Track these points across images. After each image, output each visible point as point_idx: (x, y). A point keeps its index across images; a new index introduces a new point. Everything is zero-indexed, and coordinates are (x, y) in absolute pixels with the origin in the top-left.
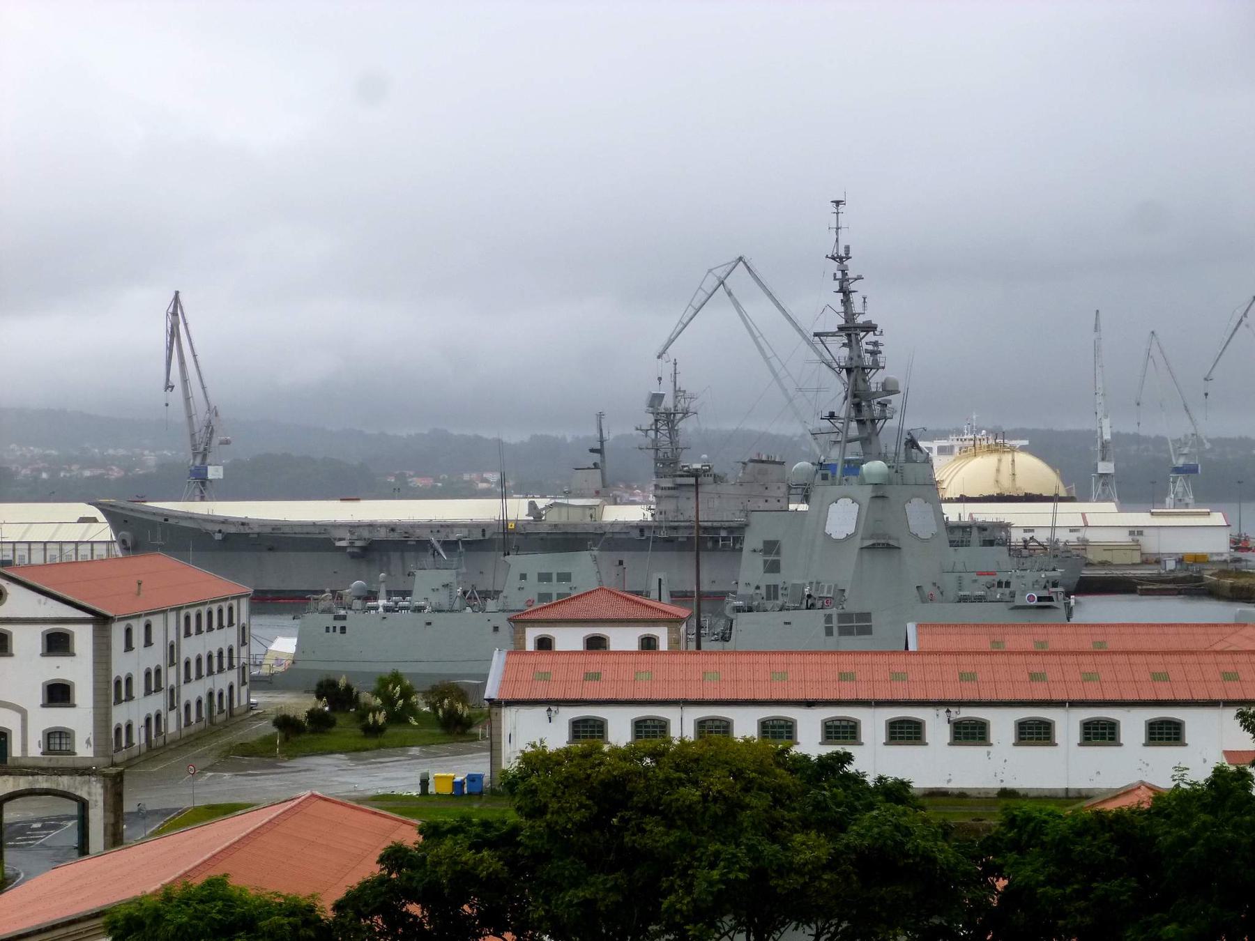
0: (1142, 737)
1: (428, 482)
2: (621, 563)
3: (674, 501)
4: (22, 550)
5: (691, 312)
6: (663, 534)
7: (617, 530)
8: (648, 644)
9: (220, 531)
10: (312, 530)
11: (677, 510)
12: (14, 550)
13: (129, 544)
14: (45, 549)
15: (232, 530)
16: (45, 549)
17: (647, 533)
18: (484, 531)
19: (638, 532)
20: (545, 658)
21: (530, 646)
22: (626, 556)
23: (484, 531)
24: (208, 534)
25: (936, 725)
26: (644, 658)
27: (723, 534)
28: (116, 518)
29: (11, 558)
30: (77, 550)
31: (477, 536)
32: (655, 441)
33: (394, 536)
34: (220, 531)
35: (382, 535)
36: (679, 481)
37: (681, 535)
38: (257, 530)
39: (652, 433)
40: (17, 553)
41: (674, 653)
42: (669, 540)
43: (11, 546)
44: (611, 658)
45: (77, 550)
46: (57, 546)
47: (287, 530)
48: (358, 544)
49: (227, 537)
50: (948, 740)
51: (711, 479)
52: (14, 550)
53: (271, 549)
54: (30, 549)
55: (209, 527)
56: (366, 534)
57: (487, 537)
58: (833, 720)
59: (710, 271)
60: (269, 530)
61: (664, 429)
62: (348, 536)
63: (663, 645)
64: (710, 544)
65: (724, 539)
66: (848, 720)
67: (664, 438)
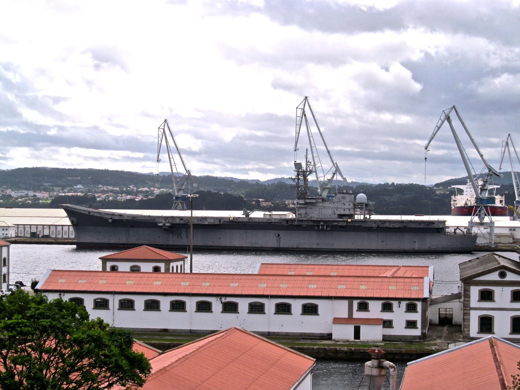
0: (143, 307)
1: (25, 186)
2: (279, 235)
3: (304, 209)
4: (40, 228)
5: (298, 127)
6: (296, 223)
7: (277, 221)
8: (156, 270)
9: (111, 218)
10: (149, 219)
11: (306, 214)
12: (37, 228)
13: (75, 223)
14: (50, 228)
15: (117, 218)
16: (50, 228)
17: (289, 223)
18: (220, 220)
19: (286, 222)
20: (114, 274)
21: (108, 269)
22: (281, 233)
23: (220, 220)
24: (106, 220)
25: (217, 305)
26: (155, 275)
27: (322, 223)
28: (71, 213)
29: (35, 231)
30: (62, 229)
31: (217, 222)
32: (298, 183)
33: (182, 222)
34: (111, 218)
35: (178, 221)
36: (308, 201)
37: (305, 224)
38: (126, 218)
39: (296, 180)
40: (38, 230)
41: (167, 273)
42: (298, 226)
43: (35, 227)
44: (141, 275)
45: (62, 229)
46: (55, 227)
47: (138, 219)
48: (167, 224)
49: (114, 221)
50: (221, 311)
51: (321, 200)
52: (37, 228)
53: (132, 227)
54: (43, 228)
55: (107, 217)
56: (171, 221)
57: (222, 223)
58: (252, 303)
59: (297, 108)
60: (131, 218)
61: (301, 177)
62: (164, 221)
63: (163, 270)
64: (316, 228)
65: (322, 226)
66: (260, 303)
67: (302, 182)
